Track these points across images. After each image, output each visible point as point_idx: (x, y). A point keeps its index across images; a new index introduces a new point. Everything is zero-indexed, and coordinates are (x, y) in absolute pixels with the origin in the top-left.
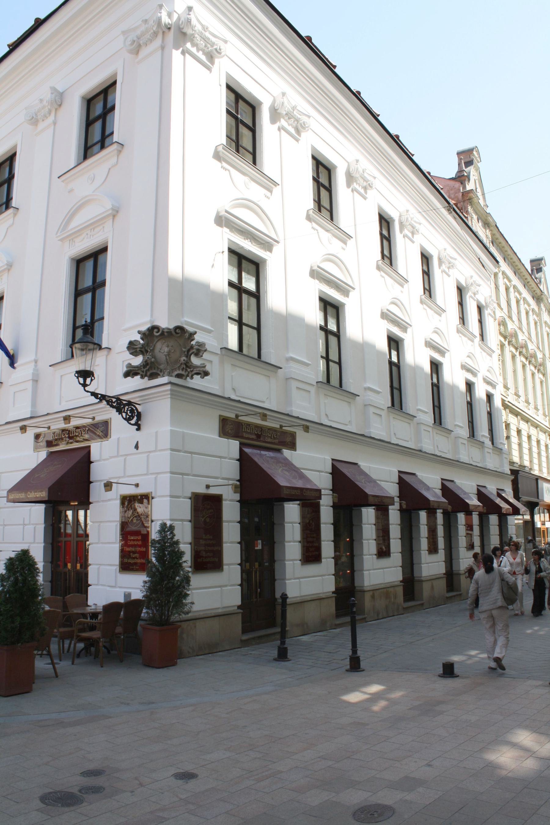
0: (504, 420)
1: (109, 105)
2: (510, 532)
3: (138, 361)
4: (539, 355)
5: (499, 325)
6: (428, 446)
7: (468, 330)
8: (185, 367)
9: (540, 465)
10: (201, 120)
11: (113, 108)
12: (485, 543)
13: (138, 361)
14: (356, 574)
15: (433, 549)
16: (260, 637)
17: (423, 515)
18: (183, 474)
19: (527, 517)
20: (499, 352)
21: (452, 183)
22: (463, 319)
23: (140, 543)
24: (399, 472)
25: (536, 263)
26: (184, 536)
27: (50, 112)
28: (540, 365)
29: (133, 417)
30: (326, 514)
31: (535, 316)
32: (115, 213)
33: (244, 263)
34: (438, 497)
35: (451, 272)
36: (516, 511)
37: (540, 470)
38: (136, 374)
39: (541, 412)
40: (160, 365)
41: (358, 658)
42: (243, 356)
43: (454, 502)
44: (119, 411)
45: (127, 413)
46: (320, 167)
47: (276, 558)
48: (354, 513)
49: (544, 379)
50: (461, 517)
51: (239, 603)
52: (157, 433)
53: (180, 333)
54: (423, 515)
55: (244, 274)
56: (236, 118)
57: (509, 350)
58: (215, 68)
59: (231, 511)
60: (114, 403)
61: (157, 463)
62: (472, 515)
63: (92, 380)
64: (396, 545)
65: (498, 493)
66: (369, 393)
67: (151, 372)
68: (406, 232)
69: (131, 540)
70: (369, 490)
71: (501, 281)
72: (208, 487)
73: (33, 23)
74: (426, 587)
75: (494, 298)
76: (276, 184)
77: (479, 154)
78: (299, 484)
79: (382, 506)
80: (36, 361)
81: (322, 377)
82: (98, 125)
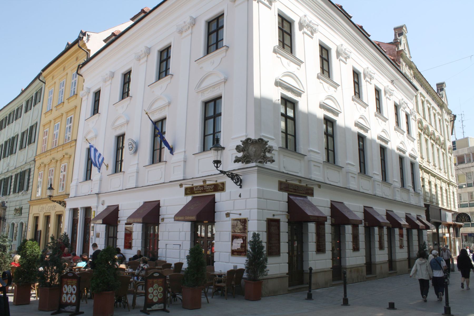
0: (421, 176)
1: (220, 26)
2: (424, 239)
3: (240, 155)
4: (442, 139)
5: (418, 123)
6: (379, 193)
7: (400, 129)
9: (442, 201)
10: (266, 32)
11: (222, 27)
12: (410, 244)
13: (240, 155)
14: (342, 259)
16: (297, 289)
17: (376, 229)
18: (263, 209)
19: (435, 231)
20: (418, 138)
21: (391, 46)
22: (398, 123)
24: (364, 207)
25: (440, 86)
26: (263, 238)
27: (189, 28)
28: (442, 144)
31: (439, 116)
32: (225, 81)
34: (384, 219)
35: (391, 98)
36: (427, 228)
37: (443, 204)
38: (240, 161)
39: (443, 171)
43: (393, 222)
44: (232, 179)
46: (323, 50)
47: (304, 250)
49: (445, 152)
50: (397, 231)
51: (287, 272)
52: (250, 190)
53: (261, 142)
54: (376, 229)
55: (288, 109)
56: (282, 30)
57: (424, 137)
58: (273, 7)
61: (248, 203)
64: (362, 245)
66: (349, 166)
68: (367, 79)
71: (419, 98)
72: (274, 215)
74: (378, 267)
75: (415, 110)
76: (302, 62)
77: (406, 29)
78: (317, 214)
79: (320, 222)
80: (185, 152)
81: (325, 159)
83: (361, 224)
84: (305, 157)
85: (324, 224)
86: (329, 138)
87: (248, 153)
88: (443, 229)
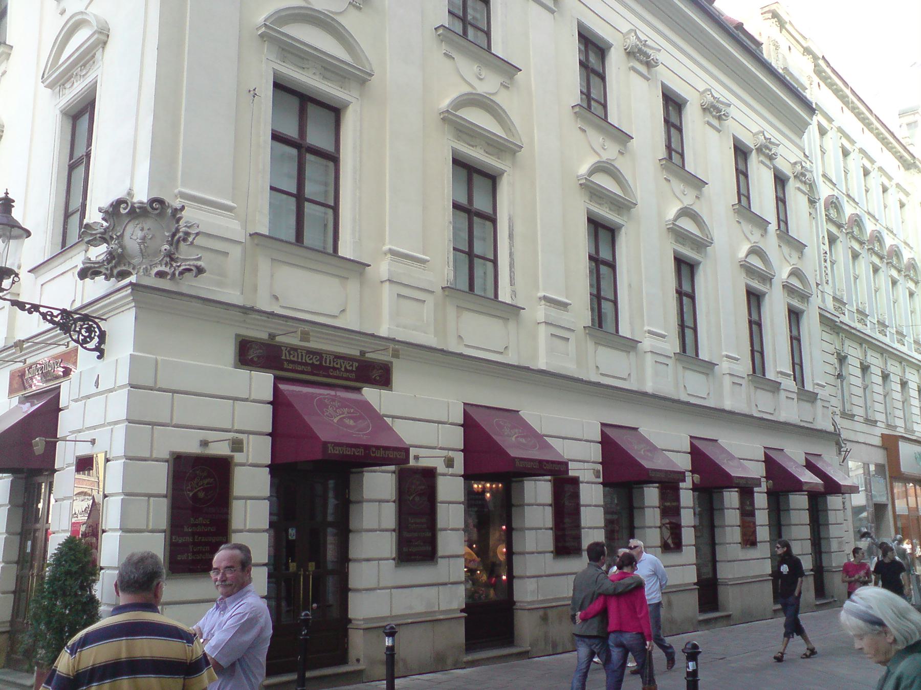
3: (98, 252)
8: (168, 260)
24: (603, 425)
29: (92, 339)
38: (96, 273)
40: (133, 258)
43: (711, 478)
48: (715, 496)
60: (56, 317)
67: (119, 269)
70: (735, 472)
72: (205, 443)
79: (746, 490)
83: (760, 486)
87: (121, 246)
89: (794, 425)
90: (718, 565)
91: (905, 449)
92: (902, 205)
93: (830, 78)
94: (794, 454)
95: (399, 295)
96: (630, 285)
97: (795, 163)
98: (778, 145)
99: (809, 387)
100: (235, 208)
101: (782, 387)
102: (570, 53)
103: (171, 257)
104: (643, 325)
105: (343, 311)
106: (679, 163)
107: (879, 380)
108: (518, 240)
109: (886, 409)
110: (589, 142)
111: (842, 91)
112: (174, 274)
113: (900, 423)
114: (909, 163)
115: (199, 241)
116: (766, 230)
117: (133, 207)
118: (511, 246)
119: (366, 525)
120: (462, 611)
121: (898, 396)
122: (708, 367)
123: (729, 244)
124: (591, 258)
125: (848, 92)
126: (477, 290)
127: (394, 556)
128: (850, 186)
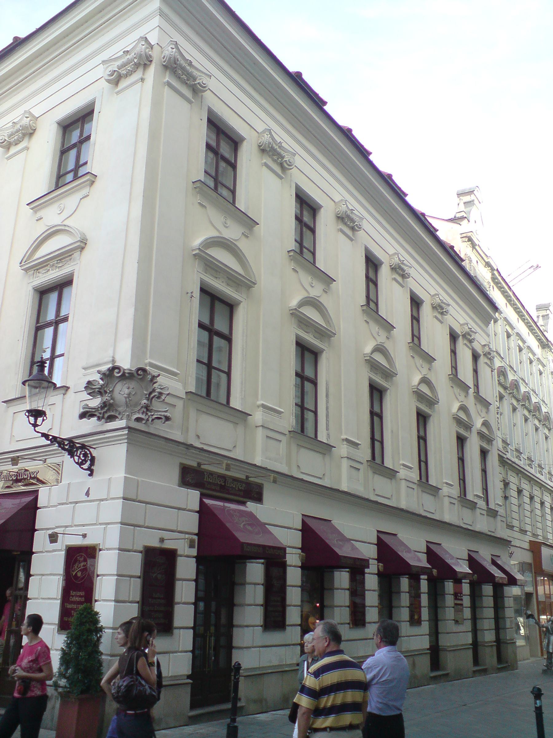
3: (96, 402)
8: (145, 410)
11: (88, 138)
13: (96, 402)
15: (415, 621)
23: (83, 599)
29: (86, 462)
30: (294, 576)
33: (218, 305)
38: (92, 415)
40: (119, 407)
41: (236, 727)
42: (211, 402)
43: (440, 569)
44: (71, 454)
45: (79, 457)
54: (405, 582)
57: (508, 401)
59: (186, 568)
60: (66, 445)
62: (461, 583)
63: (43, 420)
65: (492, 560)
67: (109, 414)
69: (73, 596)
70: (343, 551)
72: (162, 540)
73: (12, 41)
79: (357, 568)
81: (369, 457)
82: (73, 153)
84: (440, 491)
85: (363, 573)
86: (375, 418)
88: (547, 587)
89: (486, 535)
90: (440, 636)
91: (545, 551)
92: (541, 373)
93: (500, 283)
94: (485, 555)
95: (267, 437)
96: (392, 431)
97: (485, 345)
98: (476, 333)
99: (492, 506)
100: (179, 374)
101: (478, 506)
102: (290, 207)
103: (147, 408)
104: (399, 460)
105: (235, 446)
106: (418, 344)
107: (515, 494)
108: (331, 397)
109: (520, 517)
110: (299, 279)
111: (507, 292)
112: (148, 420)
113: (539, 532)
114: (545, 344)
115: (169, 400)
116: (467, 393)
117: (124, 373)
118: (327, 402)
119: (247, 602)
120: (494, 642)
121: (538, 512)
122: (391, 474)
123: (449, 402)
124: (297, 374)
125: (511, 294)
126: (213, 397)
127: (262, 624)
128: (511, 360)
